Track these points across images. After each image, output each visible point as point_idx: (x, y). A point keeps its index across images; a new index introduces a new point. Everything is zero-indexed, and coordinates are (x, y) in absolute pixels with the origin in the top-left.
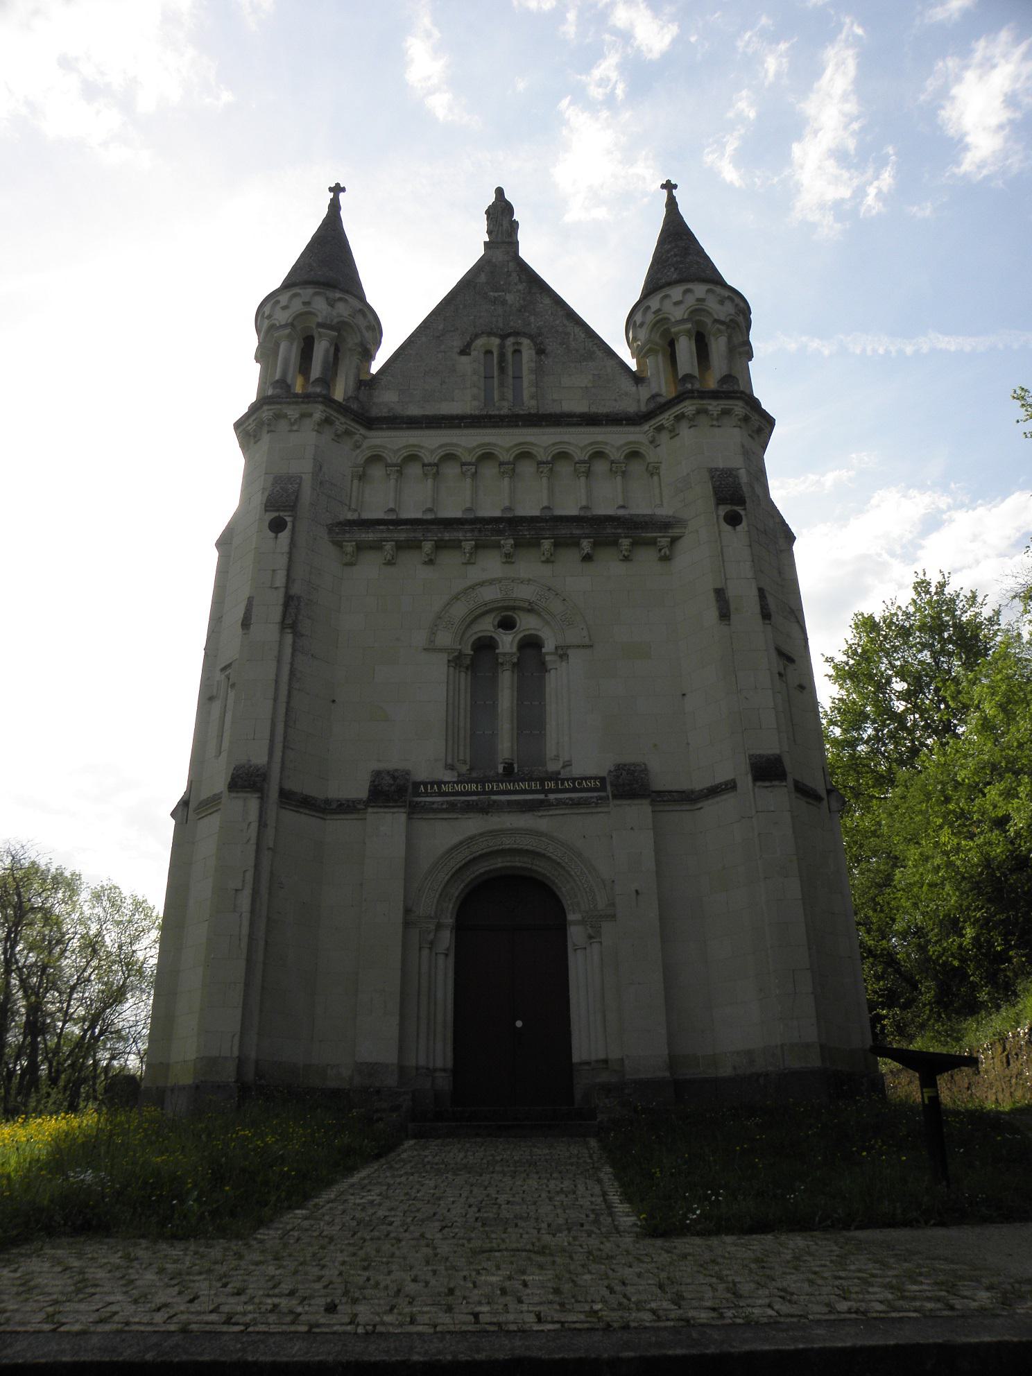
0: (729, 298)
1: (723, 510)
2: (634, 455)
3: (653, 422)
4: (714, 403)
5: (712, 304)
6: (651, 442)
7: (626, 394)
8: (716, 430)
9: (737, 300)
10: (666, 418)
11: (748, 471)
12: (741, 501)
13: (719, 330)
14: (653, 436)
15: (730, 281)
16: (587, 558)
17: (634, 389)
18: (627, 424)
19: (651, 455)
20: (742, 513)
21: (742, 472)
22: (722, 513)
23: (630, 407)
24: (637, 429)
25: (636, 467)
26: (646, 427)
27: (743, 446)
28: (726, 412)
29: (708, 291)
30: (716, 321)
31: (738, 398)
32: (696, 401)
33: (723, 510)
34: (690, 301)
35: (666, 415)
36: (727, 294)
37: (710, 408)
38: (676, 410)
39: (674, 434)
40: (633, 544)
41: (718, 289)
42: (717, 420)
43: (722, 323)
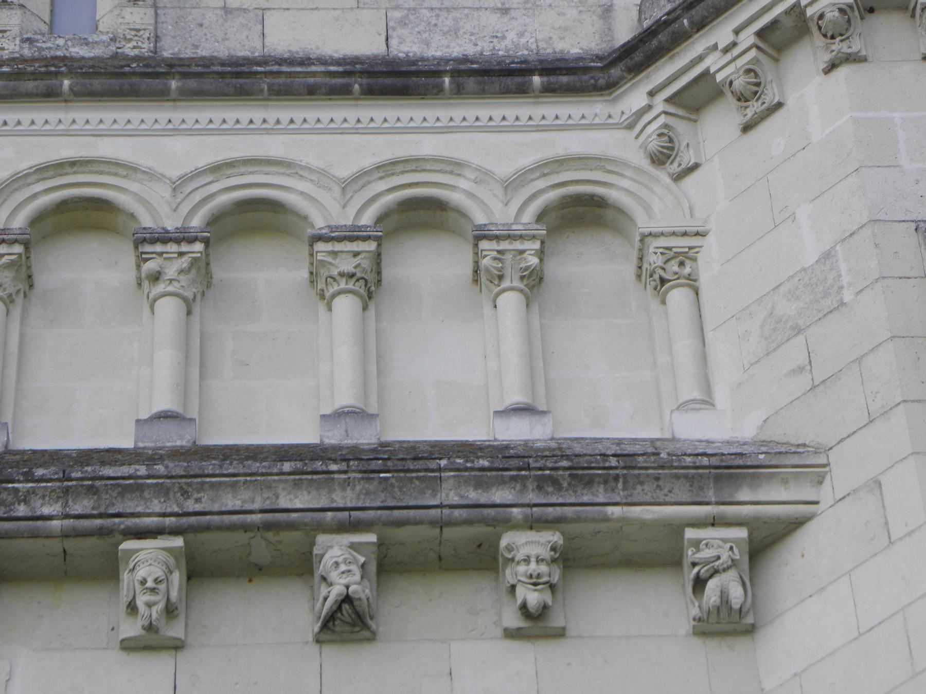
2: (582, 213)
14: (667, 134)
16: (346, 623)
18: (549, 90)
19: (653, 204)
24: (594, 109)
25: (591, 266)
26: (634, 98)
39: (757, 105)
40: (571, 560)
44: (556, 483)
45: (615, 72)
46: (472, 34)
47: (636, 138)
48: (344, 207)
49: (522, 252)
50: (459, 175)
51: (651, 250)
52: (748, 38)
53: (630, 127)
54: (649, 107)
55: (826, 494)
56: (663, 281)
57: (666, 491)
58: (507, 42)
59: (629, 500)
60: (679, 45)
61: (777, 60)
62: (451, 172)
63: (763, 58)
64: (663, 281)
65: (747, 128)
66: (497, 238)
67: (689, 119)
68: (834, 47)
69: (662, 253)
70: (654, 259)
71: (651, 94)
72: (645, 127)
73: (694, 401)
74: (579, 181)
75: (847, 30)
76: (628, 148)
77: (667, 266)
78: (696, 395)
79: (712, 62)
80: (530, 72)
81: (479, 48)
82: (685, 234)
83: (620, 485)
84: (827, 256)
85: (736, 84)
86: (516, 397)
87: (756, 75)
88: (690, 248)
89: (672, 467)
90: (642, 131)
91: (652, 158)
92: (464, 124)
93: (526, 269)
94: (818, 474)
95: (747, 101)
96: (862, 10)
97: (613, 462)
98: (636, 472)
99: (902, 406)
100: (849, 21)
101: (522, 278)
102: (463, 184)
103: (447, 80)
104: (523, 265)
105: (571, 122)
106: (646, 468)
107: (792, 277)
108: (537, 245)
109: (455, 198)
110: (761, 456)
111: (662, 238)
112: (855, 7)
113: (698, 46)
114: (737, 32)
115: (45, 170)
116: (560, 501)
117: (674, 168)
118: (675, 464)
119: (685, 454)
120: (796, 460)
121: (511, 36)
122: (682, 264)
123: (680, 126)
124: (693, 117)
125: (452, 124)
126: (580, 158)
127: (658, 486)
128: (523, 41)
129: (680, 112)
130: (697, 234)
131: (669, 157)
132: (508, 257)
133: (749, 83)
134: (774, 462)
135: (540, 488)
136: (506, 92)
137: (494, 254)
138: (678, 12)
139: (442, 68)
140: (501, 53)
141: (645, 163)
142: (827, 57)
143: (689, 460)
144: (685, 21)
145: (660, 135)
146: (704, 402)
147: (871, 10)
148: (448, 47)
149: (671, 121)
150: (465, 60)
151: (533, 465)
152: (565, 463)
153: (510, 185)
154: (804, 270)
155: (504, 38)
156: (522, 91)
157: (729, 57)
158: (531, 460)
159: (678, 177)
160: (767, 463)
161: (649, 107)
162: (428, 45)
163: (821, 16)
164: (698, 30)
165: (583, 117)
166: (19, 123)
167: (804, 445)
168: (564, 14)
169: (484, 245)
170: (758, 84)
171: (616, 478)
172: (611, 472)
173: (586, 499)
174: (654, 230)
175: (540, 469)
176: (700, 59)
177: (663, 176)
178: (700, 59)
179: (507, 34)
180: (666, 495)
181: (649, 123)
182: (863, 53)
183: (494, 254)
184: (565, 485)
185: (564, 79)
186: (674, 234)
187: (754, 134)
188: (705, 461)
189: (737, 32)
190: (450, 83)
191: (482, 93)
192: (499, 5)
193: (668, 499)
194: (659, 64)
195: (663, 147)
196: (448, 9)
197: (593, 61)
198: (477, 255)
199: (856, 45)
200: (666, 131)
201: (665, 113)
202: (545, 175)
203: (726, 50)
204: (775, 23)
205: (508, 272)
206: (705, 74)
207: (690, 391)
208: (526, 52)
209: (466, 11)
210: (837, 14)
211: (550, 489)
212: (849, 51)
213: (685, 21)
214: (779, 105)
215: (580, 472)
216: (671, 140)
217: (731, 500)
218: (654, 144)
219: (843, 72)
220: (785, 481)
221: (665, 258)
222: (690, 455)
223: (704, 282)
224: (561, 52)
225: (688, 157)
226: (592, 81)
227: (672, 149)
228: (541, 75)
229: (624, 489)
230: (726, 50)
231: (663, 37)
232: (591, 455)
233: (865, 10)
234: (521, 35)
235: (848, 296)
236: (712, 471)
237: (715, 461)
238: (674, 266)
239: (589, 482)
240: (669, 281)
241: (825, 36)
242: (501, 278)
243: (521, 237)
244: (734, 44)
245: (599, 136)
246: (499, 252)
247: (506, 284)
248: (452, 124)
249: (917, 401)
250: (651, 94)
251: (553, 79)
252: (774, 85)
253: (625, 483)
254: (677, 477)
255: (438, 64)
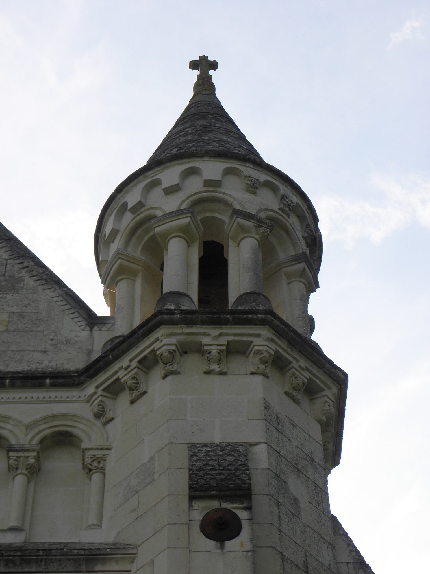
0: (267, 184)
1: (200, 510)
2: (62, 439)
3: (102, 377)
4: (214, 331)
5: (235, 192)
6: (98, 415)
7: (68, 341)
8: (217, 379)
9: (283, 189)
10: (124, 368)
11: (274, 452)
12: (243, 493)
13: (243, 229)
14: (102, 405)
15: (268, 157)
17: (86, 334)
18: (53, 385)
19: (91, 435)
20: (243, 515)
21: (261, 450)
22: (198, 516)
23: (74, 361)
24: (74, 393)
25: (63, 464)
26: (90, 389)
27: (267, 407)
28: (235, 350)
29: (228, 172)
30: (236, 212)
31: (262, 323)
32: (177, 329)
33: (200, 510)
34: (194, 186)
35: (124, 362)
36: (263, 177)
37: (205, 340)
38: (142, 348)
39: (137, 393)
41: (248, 170)
42: (219, 362)
43: (248, 216)
44: (14, 562)
45: (83, 378)
46: (28, 362)
47: (90, 406)
48: (26, 436)
49: (28, 457)
50: (8, 423)
51: (87, 456)
52: (134, 364)
53: (88, 402)
54: (95, 393)
55: (134, 567)
56: (90, 470)
57: (63, 566)
58: (43, 365)
59: (46, 570)
60: (108, 366)
61: (147, 373)
62: (4, 422)
63: (140, 372)
64: (90, 470)
65: (132, 402)
66: (17, 451)
67: (113, 398)
68: (167, 368)
69: (91, 458)
70: (88, 461)
71: (97, 387)
72: (93, 401)
73: (93, 525)
74: (61, 425)
75: (173, 360)
76: (85, 411)
77: (92, 464)
78: (95, 522)
79: (120, 374)
80: (46, 377)
81: (30, 368)
82: (102, 449)
83: (43, 563)
84: (152, 459)
85: (128, 383)
86: (13, 523)
87: (137, 380)
88: (104, 455)
89: (67, 555)
90: (92, 403)
91: (95, 415)
92: (14, 400)
93: (28, 465)
94: (132, 558)
95: (133, 390)
96: (181, 352)
97: (41, 553)
98: (51, 557)
99: (167, 527)
100: (173, 357)
101: (27, 469)
102: (9, 427)
103: (7, 381)
104: (27, 463)
105: (62, 399)
106: (56, 556)
107: (138, 468)
108: (35, 454)
109: (75, 431)
110: (108, 550)
111: (92, 451)
112: (177, 351)
113: (115, 367)
114: (131, 361)
115: (47, 419)
116: (15, 571)
117: (104, 420)
118: (69, 554)
119: (74, 549)
120: (123, 551)
121: (46, 362)
122: (99, 462)
123: (108, 402)
124: (115, 397)
125: (8, 400)
126: (63, 415)
127: (60, 564)
128: (51, 364)
129: (109, 395)
130: (107, 449)
131: (102, 414)
132: (21, 459)
133: (133, 383)
134: (114, 552)
135: (6, 565)
136: (34, 386)
137: (15, 458)
138: (109, 352)
139: (6, 376)
140: (40, 370)
141: (91, 417)
142: (163, 372)
143: (75, 551)
144: (110, 356)
145: (99, 405)
146: (98, 525)
147: (186, 352)
148: (17, 367)
149: (104, 399)
150: (14, 373)
151: (5, 554)
152: (19, 554)
153: (28, 427)
154: (143, 465)
155: (42, 363)
156: (41, 386)
157: (127, 372)
158: (4, 552)
159: (105, 424)
160: (110, 553)
161: (95, 393)
162: (7, 366)
163: (162, 355)
164: (116, 360)
165: (56, 397)
166: (38, 398)
167: (130, 545)
168: (71, 353)
169: (11, 454)
170: (137, 383)
171: (41, 560)
172: (39, 557)
173: (26, 570)
174: (88, 447)
175: (8, 556)
176: (116, 372)
177: (99, 424)
178: (116, 372)
179: (44, 362)
180: (63, 568)
181: (95, 400)
182: (179, 370)
183: (15, 458)
184: (18, 563)
185: (60, 381)
186: (97, 449)
187: (135, 405)
188: (83, 552)
189: (131, 361)
190: (9, 382)
191: (23, 386)
192: (43, 350)
193: (64, 570)
194: (100, 374)
195: (99, 410)
196: (20, 351)
197: (74, 373)
198: (9, 458)
199: (175, 367)
200: (101, 403)
201: (102, 395)
202: (46, 423)
203: (126, 369)
204: (145, 357)
205: (20, 466)
206: (118, 379)
207: (93, 520)
208: (51, 369)
209: (28, 352)
210: (167, 354)
211: (11, 565)
212: (172, 369)
213: (110, 356)
214: (145, 393)
215: (25, 557)
216: (103, 407)
217: (92, 570)
218: (96, 409)
219: (170, 378)
220: (117, 561)
221: (92, 460)
222: (77, 549)
223: (107, 471)
224: (67, 369)
225: (109, 415)
226: (72, 382)
227: (103, 411)
228: (50, 379)
229: (45, 565)
230: (126, 369)
231: (101, 363)
232: (32, 550)
233: (183, 352)
234: (50, 362)
235: (156, 477)
236: (86, 557)
237: (87, 552)
238: (95, 464)
239: (29, 562)
240: (93, 470)
241: (163, 363)
242: (17, 469)
243: (28, 450)
244: (129, 366)
245: (72, 406)
246: (17, 457)
247: (19, 471)
248: (8, 400)
249: (174, 524)
250: (97, 387)
251: (55, 380)
252: (144, 384)
253: (45, 562)
254: (69, 560)
255: (5, 374)
